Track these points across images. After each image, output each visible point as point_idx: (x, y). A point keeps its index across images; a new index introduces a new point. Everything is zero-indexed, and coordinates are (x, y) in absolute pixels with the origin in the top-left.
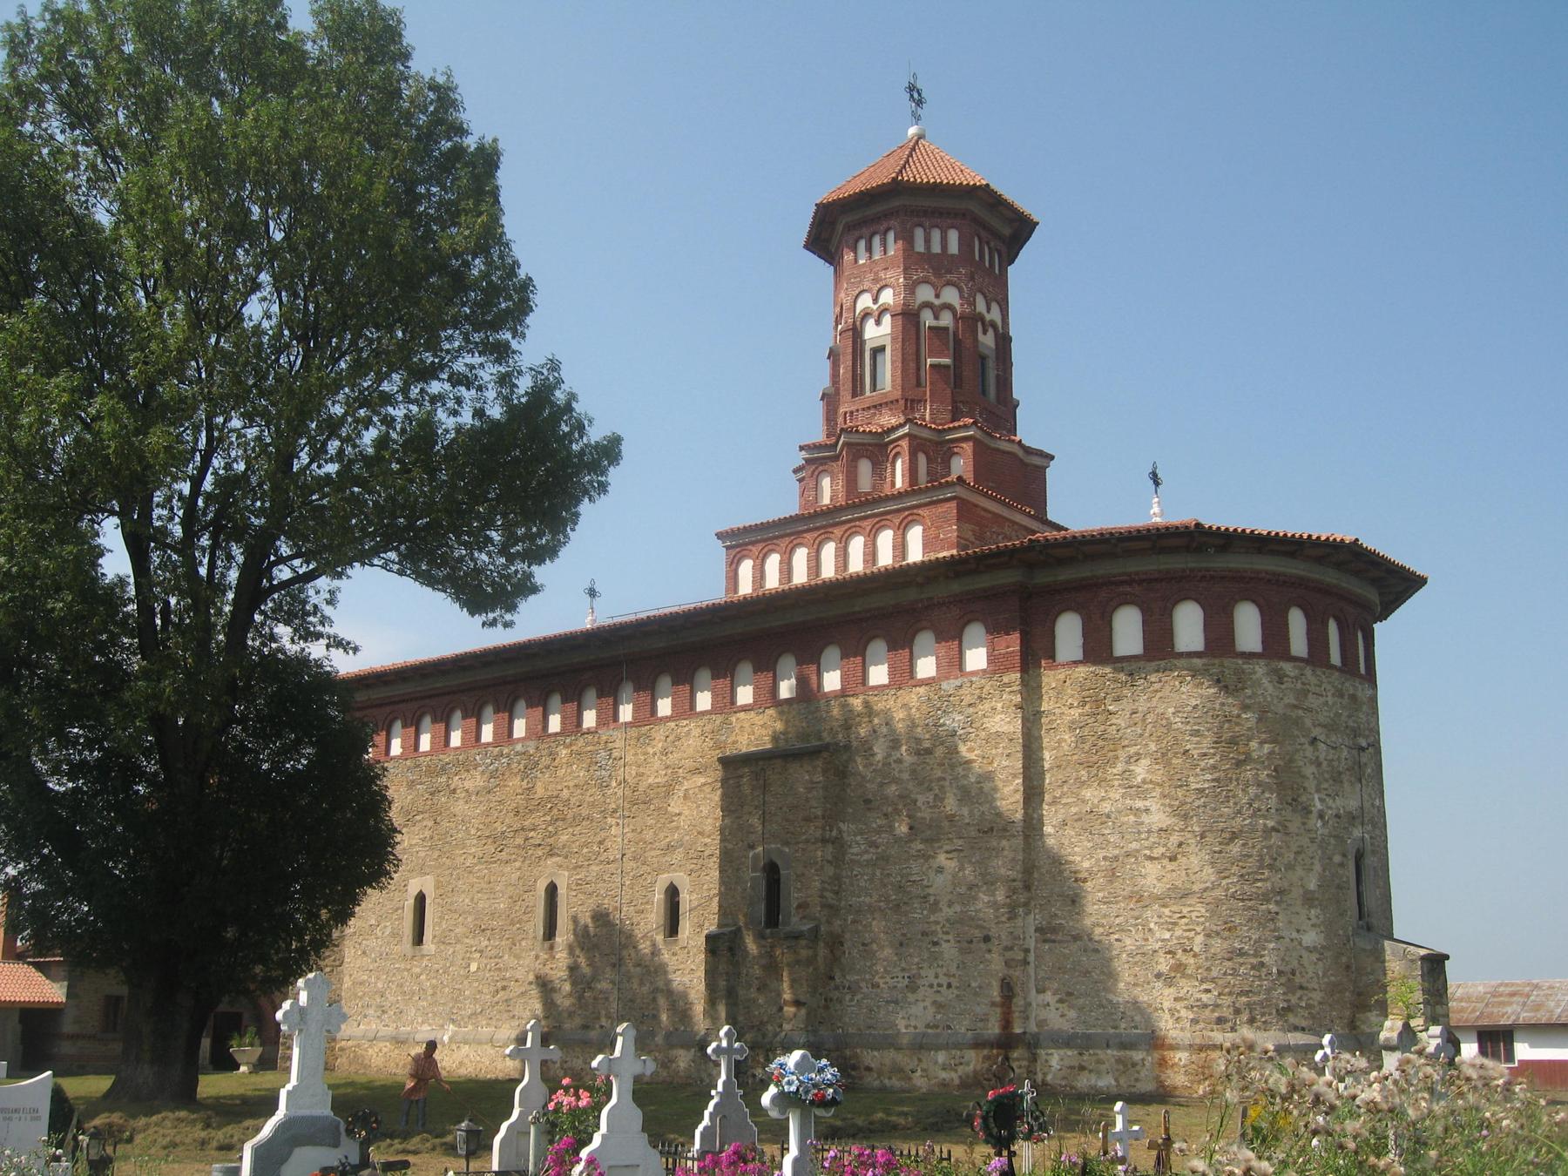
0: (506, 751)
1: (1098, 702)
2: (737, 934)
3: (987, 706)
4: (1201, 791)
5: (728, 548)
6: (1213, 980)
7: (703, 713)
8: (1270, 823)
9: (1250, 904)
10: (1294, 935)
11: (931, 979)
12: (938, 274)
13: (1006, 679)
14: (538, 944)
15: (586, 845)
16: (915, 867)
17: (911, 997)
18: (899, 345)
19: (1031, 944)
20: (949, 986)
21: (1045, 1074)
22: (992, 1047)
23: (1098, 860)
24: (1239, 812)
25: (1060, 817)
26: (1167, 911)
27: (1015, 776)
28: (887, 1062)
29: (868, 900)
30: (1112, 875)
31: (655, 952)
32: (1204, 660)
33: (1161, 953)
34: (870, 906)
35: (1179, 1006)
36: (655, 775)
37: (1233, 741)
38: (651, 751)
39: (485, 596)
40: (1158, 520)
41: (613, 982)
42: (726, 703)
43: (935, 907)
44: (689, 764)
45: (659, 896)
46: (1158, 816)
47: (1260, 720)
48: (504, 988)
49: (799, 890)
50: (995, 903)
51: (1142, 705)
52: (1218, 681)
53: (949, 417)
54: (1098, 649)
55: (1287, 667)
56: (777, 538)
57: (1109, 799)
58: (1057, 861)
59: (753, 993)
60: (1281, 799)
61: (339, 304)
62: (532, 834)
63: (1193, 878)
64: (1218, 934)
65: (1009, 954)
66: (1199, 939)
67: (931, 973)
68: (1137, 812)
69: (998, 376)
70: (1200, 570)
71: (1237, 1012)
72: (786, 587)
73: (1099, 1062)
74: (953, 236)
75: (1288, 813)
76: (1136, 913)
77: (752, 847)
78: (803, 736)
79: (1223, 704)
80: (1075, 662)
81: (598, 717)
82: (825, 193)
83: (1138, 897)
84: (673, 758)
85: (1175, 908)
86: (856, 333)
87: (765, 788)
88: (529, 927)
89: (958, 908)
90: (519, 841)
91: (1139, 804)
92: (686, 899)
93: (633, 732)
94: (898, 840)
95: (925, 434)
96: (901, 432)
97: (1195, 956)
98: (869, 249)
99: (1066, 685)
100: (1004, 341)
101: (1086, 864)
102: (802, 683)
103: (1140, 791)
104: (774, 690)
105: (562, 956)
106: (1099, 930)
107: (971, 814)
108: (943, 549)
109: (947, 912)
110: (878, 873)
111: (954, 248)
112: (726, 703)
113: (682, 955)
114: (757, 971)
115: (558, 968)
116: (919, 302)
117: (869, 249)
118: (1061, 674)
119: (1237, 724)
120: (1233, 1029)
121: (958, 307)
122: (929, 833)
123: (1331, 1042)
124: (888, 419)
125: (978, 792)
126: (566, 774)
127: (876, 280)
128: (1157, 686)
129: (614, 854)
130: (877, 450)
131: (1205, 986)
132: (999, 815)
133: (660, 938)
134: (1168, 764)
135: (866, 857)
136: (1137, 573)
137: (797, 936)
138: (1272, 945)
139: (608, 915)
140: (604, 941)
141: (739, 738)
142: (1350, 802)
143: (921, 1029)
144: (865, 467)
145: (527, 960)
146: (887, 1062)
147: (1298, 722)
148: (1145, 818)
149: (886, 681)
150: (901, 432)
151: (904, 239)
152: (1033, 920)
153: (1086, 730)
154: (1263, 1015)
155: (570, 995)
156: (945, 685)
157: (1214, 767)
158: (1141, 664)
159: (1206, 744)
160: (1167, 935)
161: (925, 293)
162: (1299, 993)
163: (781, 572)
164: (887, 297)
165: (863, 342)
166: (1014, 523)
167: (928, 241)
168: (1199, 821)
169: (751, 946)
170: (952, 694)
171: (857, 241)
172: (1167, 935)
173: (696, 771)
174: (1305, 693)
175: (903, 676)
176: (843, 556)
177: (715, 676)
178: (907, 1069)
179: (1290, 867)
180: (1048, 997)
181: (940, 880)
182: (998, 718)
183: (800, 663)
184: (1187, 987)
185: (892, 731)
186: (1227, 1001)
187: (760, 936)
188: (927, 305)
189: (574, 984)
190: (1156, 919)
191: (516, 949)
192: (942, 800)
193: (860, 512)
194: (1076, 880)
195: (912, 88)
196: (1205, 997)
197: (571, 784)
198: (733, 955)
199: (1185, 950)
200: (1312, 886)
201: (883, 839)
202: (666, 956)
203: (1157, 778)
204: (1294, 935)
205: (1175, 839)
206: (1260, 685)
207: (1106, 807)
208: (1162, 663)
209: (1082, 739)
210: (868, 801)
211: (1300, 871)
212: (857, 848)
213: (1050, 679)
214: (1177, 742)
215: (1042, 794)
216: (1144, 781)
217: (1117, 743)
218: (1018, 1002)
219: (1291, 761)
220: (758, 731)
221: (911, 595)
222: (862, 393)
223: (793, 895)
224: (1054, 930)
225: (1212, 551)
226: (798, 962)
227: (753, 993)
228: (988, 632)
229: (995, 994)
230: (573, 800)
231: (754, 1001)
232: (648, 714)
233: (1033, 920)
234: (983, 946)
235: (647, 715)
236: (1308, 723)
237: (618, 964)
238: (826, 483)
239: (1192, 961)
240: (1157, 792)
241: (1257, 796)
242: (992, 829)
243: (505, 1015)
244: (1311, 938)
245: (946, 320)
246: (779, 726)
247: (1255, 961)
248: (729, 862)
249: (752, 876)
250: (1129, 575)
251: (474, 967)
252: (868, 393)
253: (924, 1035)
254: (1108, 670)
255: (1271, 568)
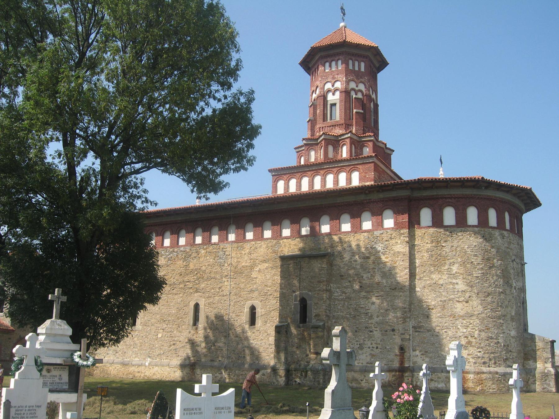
0: (176, 250)
1: (438, 242)
2: (288, 326)
3: (394, 241)
4: (477, 277)
5: (273, 176)
6: (482, 348)
7: (267, 239)
8: (501, 290)
9: (494, 320)
10: (508, 332)
11: (369, 345)
12: (358, 79)
13: (402, 231)
14: (190, 328)
15: (213, 288)
16: (362, 302)
17: (360, 352)
18: (343, 103)
19: (411, 332)
20: (377, 348)
21: (417, 382)
22: (396, 371)
23: (438, 302)
24: (490, 286)
25: (423, 285)
26: (465, 322)
27: (406, 268)
28: (350, 377)
29: (341, 314)
30: (443, 308)
31: (244, 331)
32: (479, 229)
33: (462, 337)
34: (342, 316)
35: (469, 357)
36: (245, 262)
37: (488, 259)
38: (243, 252)
39: (206, 183)
40: (443, 176)
41: (225, 343)
42: (277, 236)
43: (371, 317)
44: (261, 258)
45: (247, 310)
46: (461, 286)
47: (497, 252)
48: (174, 344)
49: (316, 309)
50: (397, 317)
51: (455, 244)
52: (483, 237)
53: (362, 132)
54: (437, 222)
55: (505, 233)
56: (295, 173)
57: (443, 279)
58: (420, 301)
59: (294, 349)
60: (504, 281)
61: (141, 56)
62: (187, 283)
63: (475, 309)
64: (483, 330)
65: (402, 336)
66: (477, 332)
67: (369, 343)
68: (453, 284)
69: (374, 119)
70: (477, 195)
71: (490, 360)
72: (298, 192)
73: (439, 378)
74: (363, 65)
75: (506, 287)
76: (453, 322)
77: (294, 292)
78: (311, 249)
79: (485, 245)
80: (429, 227)
81: (219, 238)
82: (315, 42)
83: (453, 316)
84: (253, 256)
85: (468, 321)
86: (324, 97)
87: (300, 269)
88: (186, 320)
89: (381, 318)
90: (182, 286)
91: (454, 281)
92: (259, 311)
93: (235, 245)
94: (354, 291)
95: (355, 137)
96: (346, 136)
97: (475, 338)
98: (330, 66)
99: (425, 235)
100: (376, 106)
101: (433, 303)
102: (312, 229)
103: (454, 276)
104: (299, 231)
105: (201, 332)
106: (438, 328)
107: (387, 282)
108: (368, 181)
109: (376, 319)
110: (346, 303)
111: (363, 69)
112: (277, 236)
113: (257, 333)
114: (296, 340)
115: (199, 337)
116: (350, 88)
117: (330, 66)
118: (423, 231)
119: (490, 253)
120: (489, 367)
121: (364, 91)
122: (368, 289)
123: (426, 367)
124: (338, 131)
125: (389, 273)
126: (204, 260)
127: (333, 78)
128: (461, 237)
129: (226, 292)
130: (335, 142)
131: (479, 350)
132: (398, 283)
133: (247, 327)
134: (465, 266)
135: (341, 297)
136: (454, 195)
137: (317, 327)
138: (501, 335)
139: (223, 316)
140: (220, 327)
141: (284, 249)
142: (520, 284)
143: (365, 364)
144: (331, 148)
145: (185, 333)
146: (350, 377)
147: (508, 254)
148: (456, 286)
149: (270, 237)
150: (346, 136)
151: (346, 64)
152: (411, 323)
153: (433, 253)
154: (499, 361)
155: (205, 347)
156: (375, 233)
157: (482, 269)
158: (455, 229)
159: (479, 259)
160: (465, 331)
161: (352, 85)
162: (510, 353)
163: (347, 179)
164: (338, 85)
165: (327, 101)
166: (388, 174)
167: (354, 65)
168: (477, 288)
169: (294, 330)
170: (381, 236)
171: (325, 63)
172: (465, 331)
173: (264, 261)
174: (510, 243)
175: (357, 229)
176: (324, 182)
177: (273, 225)
178: (359, 379)
179: (507, 307)
180: (417, 353)
181: (373, 307)
182: (398, 246)
183: (311, 221)
184: (472, 350)
185: (352, 249)
186: (486, 356)
187: (298, 327)
188: (353, 89)
189: (207, 343)
190: (460, 324)
191: (180, 329)
192: (374, 277)
193: (330, 165)
194: (429, 309)
195: (342, 8)
196: (479, 354)
197: (206, 264)
198: (287, 334)
199: (471, 336)
200: (513, 314)
201: (349, 290)
202: (249, 334)
203: (461, 272)
204: (508, 332)
205: (468, 295)
206: (497, 239)
207: (441, 282)
208: (463, 229)
209: (432, 256)
210: (342, 276)
211: (510, 309)
212: (337, 294)
213: (418, 232)
214: (468, 258)
215: (415, 275)
216: (456, 273)
217: (445, 258)
218: (406, 355)
219: (507, 268)
220: (292, 247)
221: (362, 197)
222: (327, 121)
223: (313, 311)
224: (420, 327)
225: (483, 188)
226: (318, 337)
227: (294, 349)
228: (395, 213)
229: (397, 351)
230: (207, 271)
231: (295, 352)
232: (260, 236)
233: (411, 323)
234: (391, 332)
235: (241, 239)
236: (511, 254)
237: (227, 336)
238: (313, 153)
239: (474, 340)
240: (461, 277)
241: (496, 280)
242: (396, 288)
243: (174, 355)
244: (513, 333)
245: (360, 96)
246: (301, 245)
247: (496, 341)
248: (283, 298)
249: (294, 304)
250: (451, 195)
251: (160, 335)
252: (329, 121)
253: (366, 366)
254: (442, 230)
255: (501, 196)
